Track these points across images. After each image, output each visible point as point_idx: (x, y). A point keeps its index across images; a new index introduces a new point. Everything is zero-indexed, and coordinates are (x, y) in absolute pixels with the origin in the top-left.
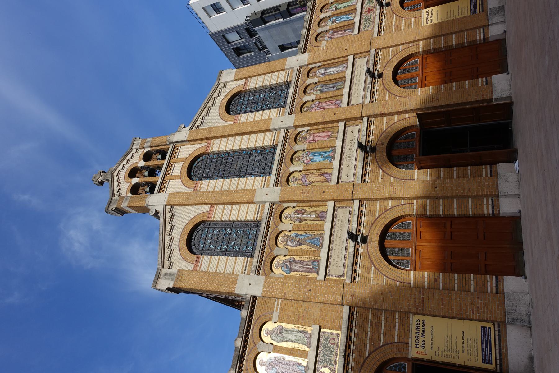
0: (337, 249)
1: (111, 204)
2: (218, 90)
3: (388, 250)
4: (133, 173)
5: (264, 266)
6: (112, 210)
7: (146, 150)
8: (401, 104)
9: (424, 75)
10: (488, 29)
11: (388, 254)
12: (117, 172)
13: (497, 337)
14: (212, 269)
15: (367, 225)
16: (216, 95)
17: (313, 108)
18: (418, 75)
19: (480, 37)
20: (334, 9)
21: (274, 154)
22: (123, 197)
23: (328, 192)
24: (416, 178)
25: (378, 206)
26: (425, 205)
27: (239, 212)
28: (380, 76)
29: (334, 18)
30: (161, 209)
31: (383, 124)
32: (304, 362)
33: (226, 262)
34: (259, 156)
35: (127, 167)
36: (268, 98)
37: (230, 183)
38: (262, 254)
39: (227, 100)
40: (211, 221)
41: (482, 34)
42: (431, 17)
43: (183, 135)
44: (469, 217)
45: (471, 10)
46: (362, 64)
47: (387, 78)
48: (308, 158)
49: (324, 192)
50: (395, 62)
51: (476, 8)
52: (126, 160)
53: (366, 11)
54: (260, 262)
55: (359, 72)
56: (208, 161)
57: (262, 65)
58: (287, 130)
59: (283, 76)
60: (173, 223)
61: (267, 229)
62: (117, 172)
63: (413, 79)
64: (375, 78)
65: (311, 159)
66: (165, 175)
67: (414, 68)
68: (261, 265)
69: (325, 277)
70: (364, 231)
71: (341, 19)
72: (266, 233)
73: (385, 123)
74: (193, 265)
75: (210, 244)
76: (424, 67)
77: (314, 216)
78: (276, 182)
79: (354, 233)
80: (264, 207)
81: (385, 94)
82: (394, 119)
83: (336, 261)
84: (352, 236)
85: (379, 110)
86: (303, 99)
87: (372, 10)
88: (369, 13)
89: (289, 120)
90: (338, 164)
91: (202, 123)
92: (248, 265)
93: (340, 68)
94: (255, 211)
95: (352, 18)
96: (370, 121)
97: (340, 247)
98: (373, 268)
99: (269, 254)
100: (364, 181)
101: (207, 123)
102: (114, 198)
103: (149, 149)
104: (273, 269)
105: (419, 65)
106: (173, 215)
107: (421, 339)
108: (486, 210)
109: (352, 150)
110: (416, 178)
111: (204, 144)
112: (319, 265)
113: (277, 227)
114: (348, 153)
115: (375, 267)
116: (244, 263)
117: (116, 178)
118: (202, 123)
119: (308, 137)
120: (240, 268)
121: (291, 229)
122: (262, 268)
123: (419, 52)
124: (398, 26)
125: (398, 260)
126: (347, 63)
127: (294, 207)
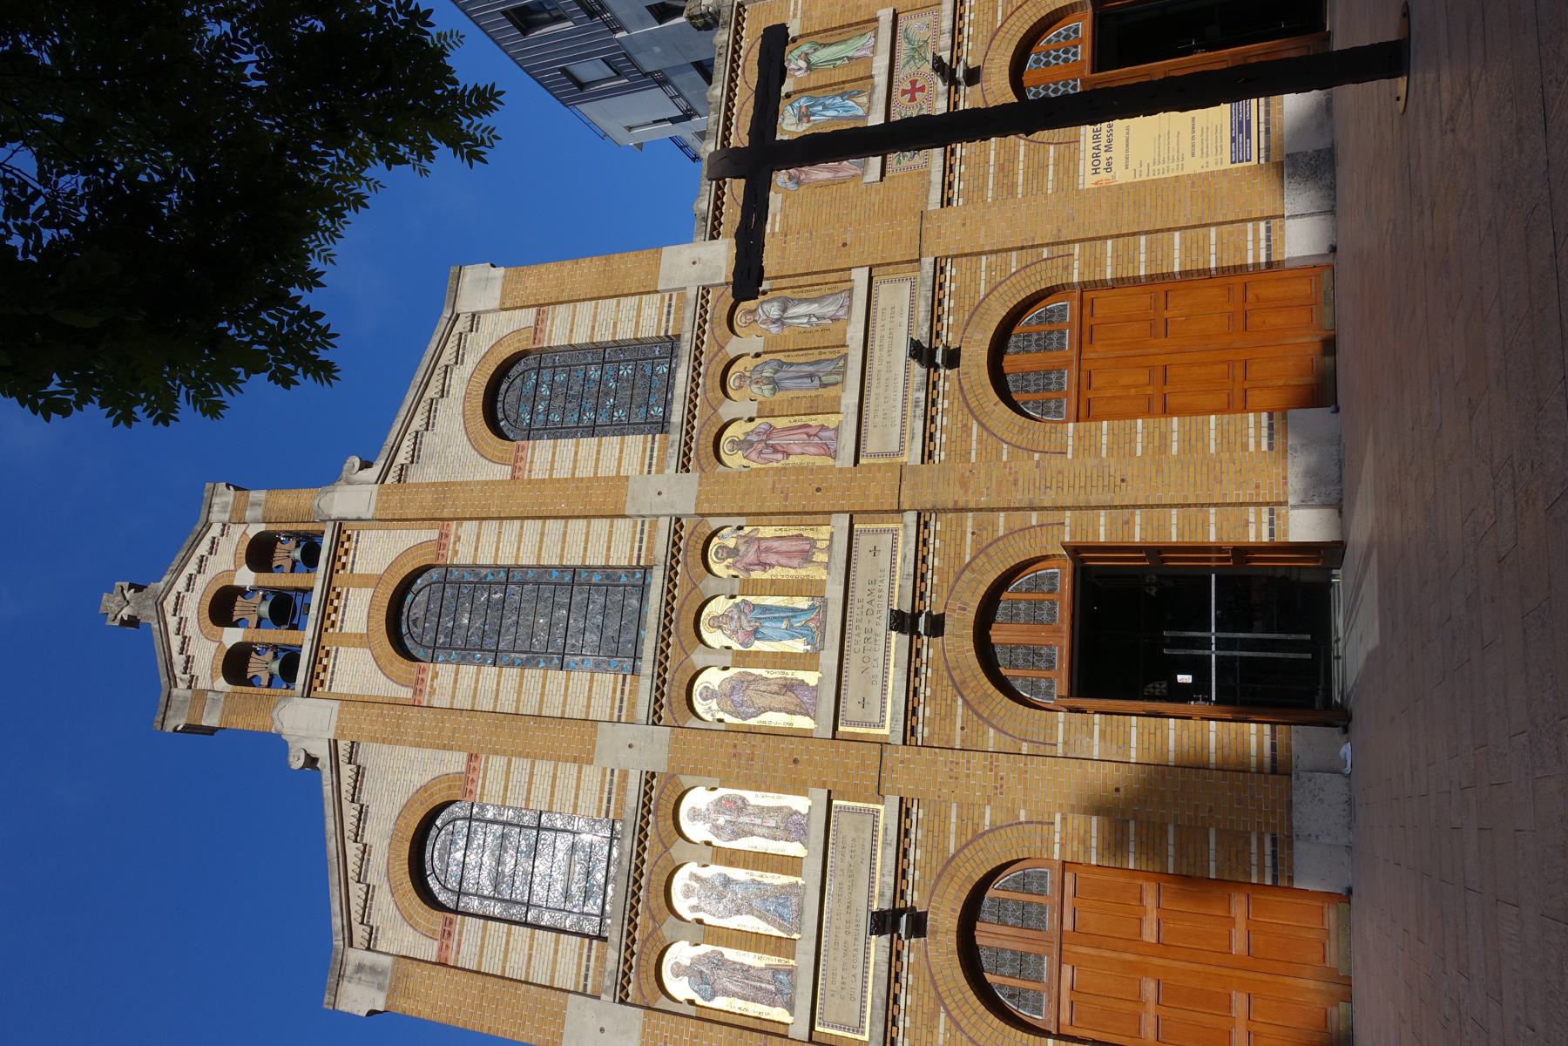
0: (841, 943)
1: (170, 713)
2: (453, 340)
3: (984, 954)
4: (223, 607)
5: (702, 449)
6: (175, 730)
7: (254, 530)
8: (1015, 483)
9: (1086, 366)
10: (1282, 228)
11: (1012, 389)
12: (171, 598)
13: (1262, 135)
14: (563, 472)
15: (923, 877)
16: (448, 356)
17: (751, 444)
18: (1068, 364)
19: (1256, 256)
20: (803, 64)
21: (643, 589)
22: (204, 692)
23: (810, 762)
24: (1060, 739)
25: (954, 819)
26: (1087, 831)
27: (553, 786)
28: (953, 359)
29: (803, 102)
30: (321, 752)
31: (963, 538)
32: (811, 678)
33: (531, 948)
34: (597, 591)
35: (201, 582)
36: (612, 384)
37: (521, 685)
38: (629, 934)
39: (485, 381)
40: (542, 351)
41: (1263, 244)
42: (1109, 149)
43: (352, 496)
44: (1205, 767)
45: (1233, 140)
46: (900, 312)
47: (974, 371)
48: (744, 622)
49: (796, 761)
50: (998, 312)
51: (1249, 136)
52: (194, 560)
53: (904, 92)
54: (626, 961)
55: (886, 333)
56: (449, 591)
57: (585, 263)
58: (678, 520)
59: (654, 312)
60: (364, 798)
61: (639, 855)
62: (171, 598)
63: (1053, 376)
64: (937, 367)
65: (756, 631)
66: (321, 630)
67: (1055, 336)
68: (631, 968)
69: (835, 728)
70: (950, 338)
71: (825, 108)
72: (637, 868)
73: (969, 536)
74: (436, 944)
75: (548, 411)
76: (1086, 338)
77: (772, 823)
78: (657, 700)
79: (926, 345)
80: (653, 526)
81: (966, 429)
82: (994, 524)
83: (839, 979)
84: (902, 622)
85: (951, 495)
86: (721, 411)
87: (922, 89)
88: (913, 99)
89: (678, 493)
90: (836, 662)
91: (414, 458)
92: (592, 964)
93: (829, 309)
94: (602, 790)
95: (861, 112)
96: (926, 525)
97: (850, 939)
98: (943, 1016)
99: (650, 935)
100: (949, 202)
101: (431, 456)
102: (175, 692)
103: (262, 528)
104: (736, 328)
105: (1070, 325)
106: (359, 773)
107: (1104, 156)
108: (1250, 254)
109: (874, 618)
110: (1060, 739)
111: (429, 534)
112: (793, 986)
113: (666, 849)
114: (863, 625)
115: (948, 1013)
116: (580, 955)
117: (172, 622)
118: (414, 458)
119: (742, 548)
120: (636, 461)
121: (760, 350)
122: (632, 976)
123: (1071, 285)
124: (1007, 187)
125: (1011, 987)
126: (876, 29)
127: (740, 528)
